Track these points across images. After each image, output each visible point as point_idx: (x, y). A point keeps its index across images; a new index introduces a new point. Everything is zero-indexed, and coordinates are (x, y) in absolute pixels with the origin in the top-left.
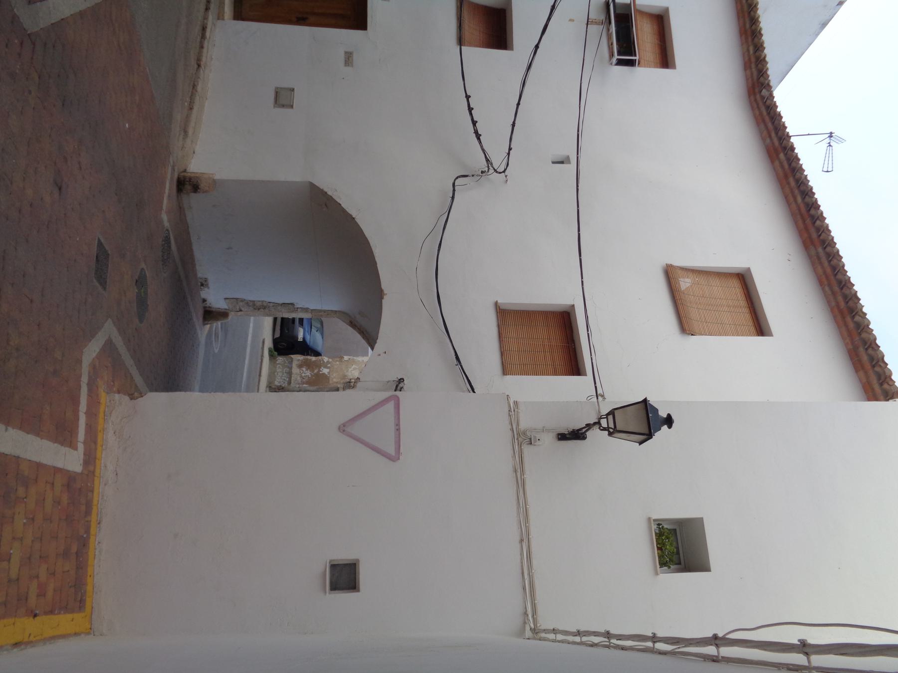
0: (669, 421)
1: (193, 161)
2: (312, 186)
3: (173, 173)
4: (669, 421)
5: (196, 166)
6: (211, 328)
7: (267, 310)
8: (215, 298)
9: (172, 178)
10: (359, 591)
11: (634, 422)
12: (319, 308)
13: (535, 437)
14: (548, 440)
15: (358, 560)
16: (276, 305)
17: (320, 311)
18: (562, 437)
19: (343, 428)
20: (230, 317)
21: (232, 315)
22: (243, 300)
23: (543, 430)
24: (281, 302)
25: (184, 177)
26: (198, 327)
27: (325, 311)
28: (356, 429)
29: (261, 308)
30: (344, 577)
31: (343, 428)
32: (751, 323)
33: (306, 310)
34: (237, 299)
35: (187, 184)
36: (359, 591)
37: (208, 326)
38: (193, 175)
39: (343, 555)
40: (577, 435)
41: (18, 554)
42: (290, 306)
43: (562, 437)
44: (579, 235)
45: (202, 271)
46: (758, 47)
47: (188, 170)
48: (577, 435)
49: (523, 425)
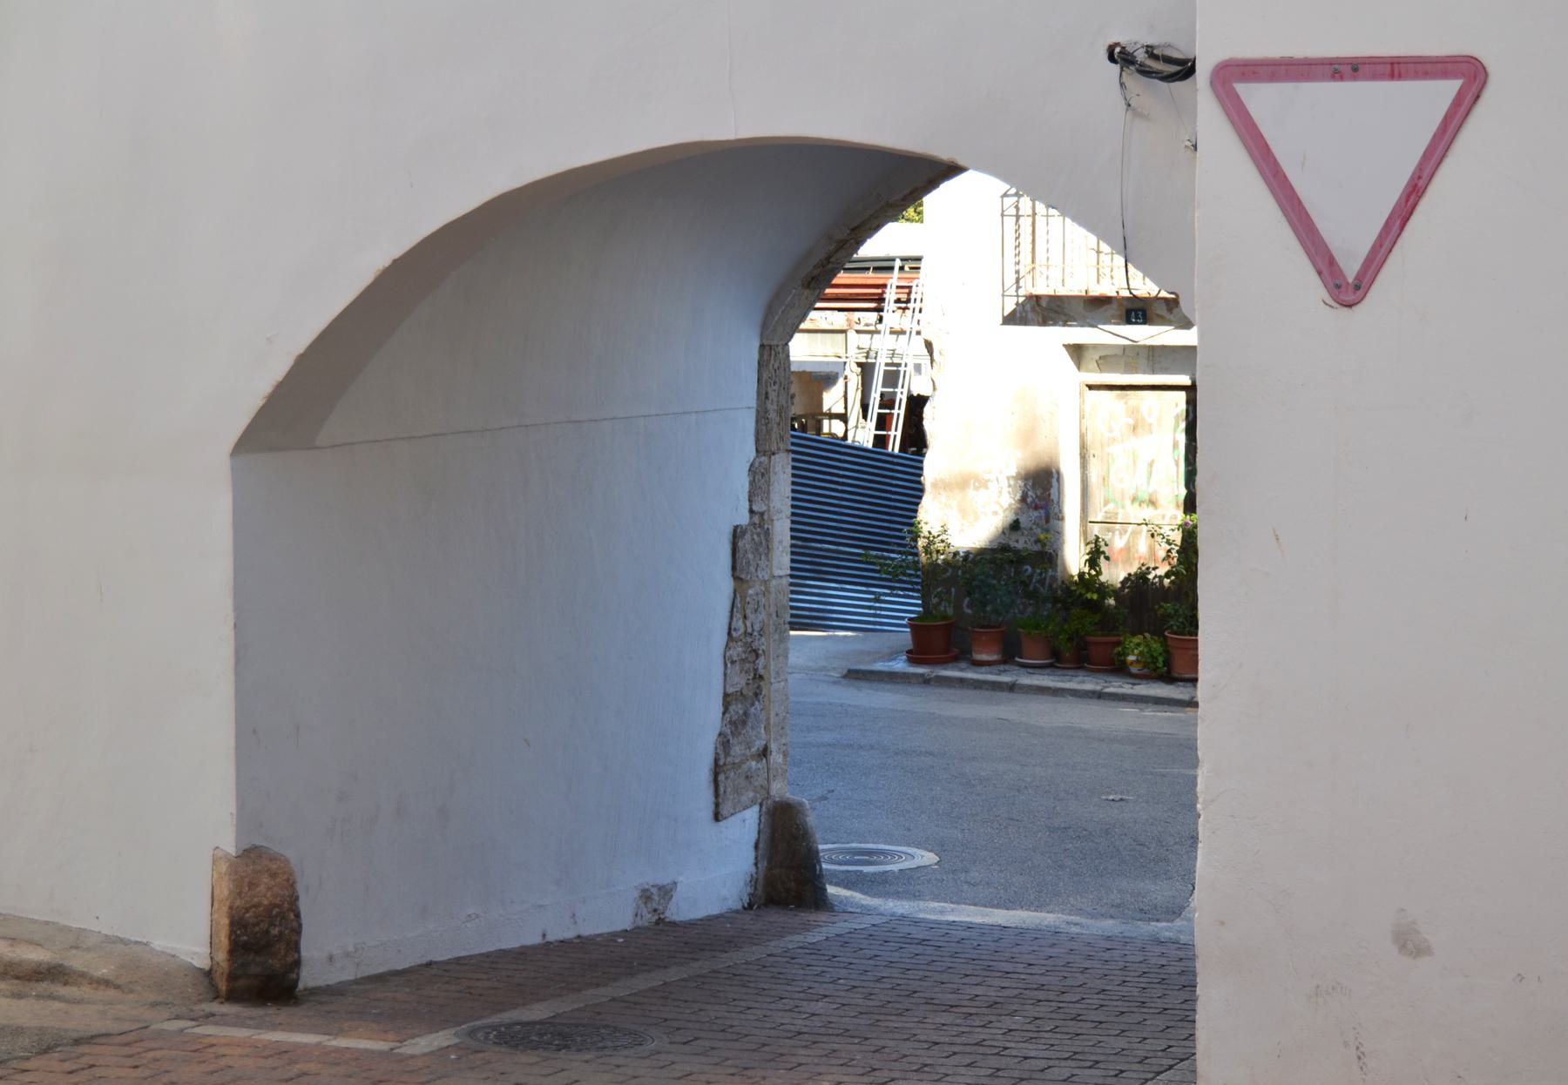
1: (158, 944)
2: (249, 442)
3: (223, 1021)
5: (189, 933)
6: (849, 882)
7: (761, 644)
8: (715, 869)
9: (239, 1022)
12: (748, 422)
16: (739, 605)
17: (762, 416)
20: (791, 796)
21: (779, 789)
22: (724, 743)
24: (726, 585)
25: (232, 977)
26: (841, 926)
27: (763, 396)
29: (748, 658)
31: (1347, 290)
32: (1114, 704)
33: (759, 477)
35: (260, 960)
37: (831, 890)
38: (223, 939)
42: (745, 546)
44: (1414, 192)
45: (609, 912)
47: (203, 962)
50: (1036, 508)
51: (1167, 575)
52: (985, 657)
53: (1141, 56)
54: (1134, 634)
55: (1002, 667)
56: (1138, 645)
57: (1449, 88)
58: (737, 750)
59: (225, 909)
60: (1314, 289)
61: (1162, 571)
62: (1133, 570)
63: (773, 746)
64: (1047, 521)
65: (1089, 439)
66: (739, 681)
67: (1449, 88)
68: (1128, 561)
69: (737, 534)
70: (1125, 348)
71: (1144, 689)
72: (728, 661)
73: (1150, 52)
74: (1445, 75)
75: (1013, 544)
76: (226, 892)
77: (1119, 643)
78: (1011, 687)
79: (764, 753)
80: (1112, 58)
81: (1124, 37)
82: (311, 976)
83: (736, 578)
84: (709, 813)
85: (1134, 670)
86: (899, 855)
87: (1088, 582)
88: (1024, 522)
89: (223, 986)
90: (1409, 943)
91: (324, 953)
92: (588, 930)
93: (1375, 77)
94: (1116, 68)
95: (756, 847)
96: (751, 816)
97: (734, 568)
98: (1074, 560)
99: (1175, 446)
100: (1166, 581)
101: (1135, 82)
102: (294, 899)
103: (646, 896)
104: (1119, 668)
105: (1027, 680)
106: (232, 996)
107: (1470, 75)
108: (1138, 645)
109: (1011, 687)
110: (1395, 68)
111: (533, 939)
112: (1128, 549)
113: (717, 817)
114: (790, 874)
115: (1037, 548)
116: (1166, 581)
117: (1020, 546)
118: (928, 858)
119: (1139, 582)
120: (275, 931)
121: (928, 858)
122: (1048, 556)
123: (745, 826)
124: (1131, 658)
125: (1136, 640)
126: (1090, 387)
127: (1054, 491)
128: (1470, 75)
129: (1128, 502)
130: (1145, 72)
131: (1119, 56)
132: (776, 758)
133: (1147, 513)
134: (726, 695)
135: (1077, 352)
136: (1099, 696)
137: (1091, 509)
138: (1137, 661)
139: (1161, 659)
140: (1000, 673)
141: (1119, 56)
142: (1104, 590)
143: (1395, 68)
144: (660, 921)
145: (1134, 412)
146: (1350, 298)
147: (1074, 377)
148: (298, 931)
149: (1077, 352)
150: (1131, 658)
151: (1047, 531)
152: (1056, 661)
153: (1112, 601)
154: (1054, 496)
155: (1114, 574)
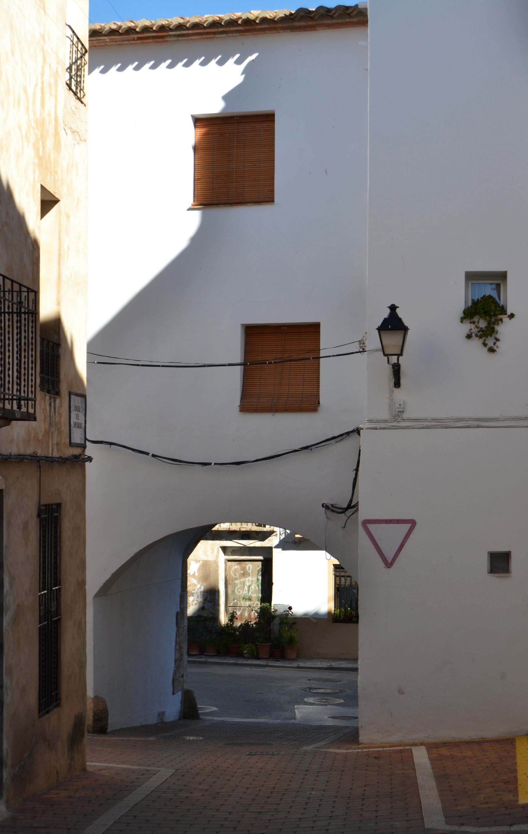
0: (393, 308)
4: (393, 308)
8: (172, 708)
10: (510, 552)
11: (392, 340)
13: (398, 408)
14: (400, 395)
15: (489, 552)
18: (327, 174)
19: (389, 564)
21: (186, 687)
22: (175, 673)
23: (391, 399)
24: (175, 628)
28: (390, 556)
30: (500, 563)
31: (389, 564)
34: (174, 680)
36: (510, 552)
39: (484, 563)
40: (396, 370)
41: (474, 767)
43: (397, 384)
46: (398, 523)
48: (396, 370)
49: (386, 415)
50: (210, 602)
51: (255, 623)
52: (194, 653)
53: (330, 506)
54: (246, 644)
55: (200, 656)
56: (248, 647)
57: (408, 526)
58: (178, 675)
59: (92, 711)
60: (382, 565)
61: (253, 623)
62: (243, 622)
63: (185, 674)
64: (214, 606)
65: (228, 578)
66: (178, 655)
67: (408, 526)
68: (241, 619)
69: (177, 614)
70: (240, 547)
71: (250, 662)
72: (176, 650)
73: (332, 505)
74: (408, 523)
75: (202, 615)
76: (92, 706)
77: (240, 647)
78: (205, 663)
79: (183, 676)
80: (323, 506)
81: (325, 502)
82: (109, 729)
83: (177, 627)
84: (171, 693)
85: (246, 656)
86: (207, 708)
87: (229, 626)
88: (206, 606)
89: (91, 730)
90: (401, 692)
91: (114, 721)
92: (149, 723)
93: (394, 523)
94: (324, 509)
95: (181, 702)
96: (180, 693)
97: (177, 624)
98: (223, 619)
99: (258, 580)
100: (254, 625)
101: (329, 513)
102: (106, 708)
103: (159, 715)
104: (240, 655)
105: (210, 660)
106: (93, 732)
107: (413, 523)
108: (248, 647)
109: (205, 663)
110: (398, 522)
111: (139, 725)
112: (241, 615)
113: (174, 694)
114: (190, 710)
115: (210, 616)
116: (254, 625)
117: (205, 615)
118: (215, 709)
119: (246, 625)
120: (103, 716)
121: (215, 709)
122: (216, 618)
123: (179, 696)
124: (245, 652)
125: (246, 646)
126: (229, 561)
127: (217, 596)
128: (413, 523)
129: (241, 600)
130: (333, 511)
131: (325, 506)
132: (185, 677)
133: (248, 603)
134: (175, 659)
135: (224, 549)
136: (236, 664)
137: (228, 602)
138: (247, 653)
139: (255, 652)
140: (200, 658)
141: (325, 506)
142: (235, 629)
143: (398, 522)
144: (162, 722)
145: (244, 569)
146: (389, 566)
147: (222, 557)
148: (108, 716)
149: (224, 549)
150: (245, 652)
151: (214, 610)
152: (218, 654)
153: (238, 633)
154: (217, 598)
155: (238, 624)
